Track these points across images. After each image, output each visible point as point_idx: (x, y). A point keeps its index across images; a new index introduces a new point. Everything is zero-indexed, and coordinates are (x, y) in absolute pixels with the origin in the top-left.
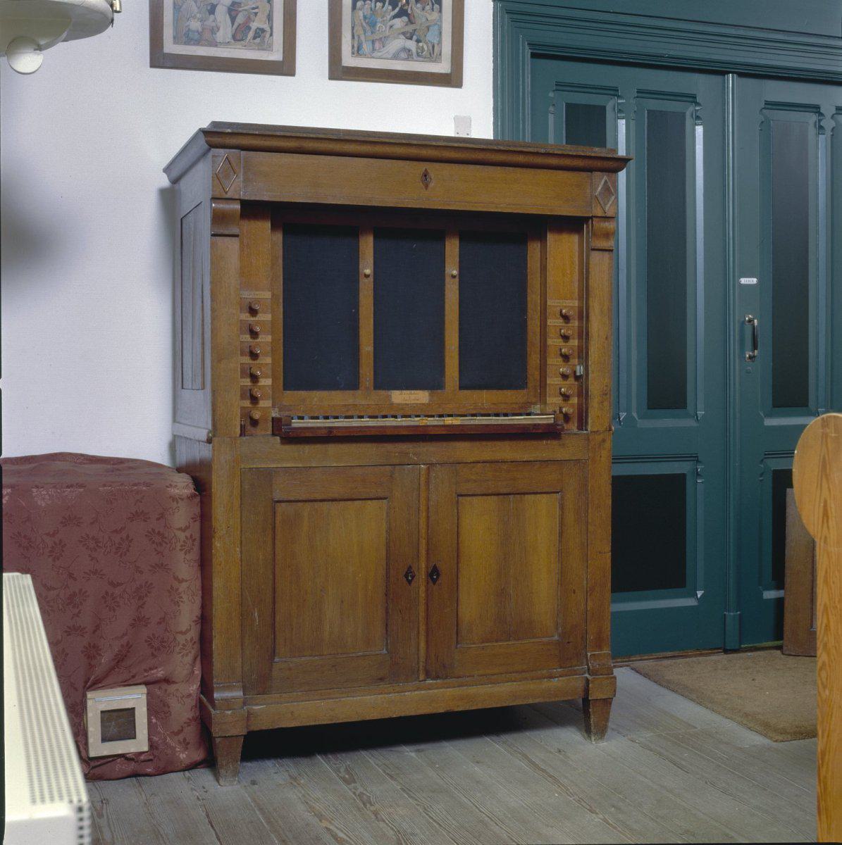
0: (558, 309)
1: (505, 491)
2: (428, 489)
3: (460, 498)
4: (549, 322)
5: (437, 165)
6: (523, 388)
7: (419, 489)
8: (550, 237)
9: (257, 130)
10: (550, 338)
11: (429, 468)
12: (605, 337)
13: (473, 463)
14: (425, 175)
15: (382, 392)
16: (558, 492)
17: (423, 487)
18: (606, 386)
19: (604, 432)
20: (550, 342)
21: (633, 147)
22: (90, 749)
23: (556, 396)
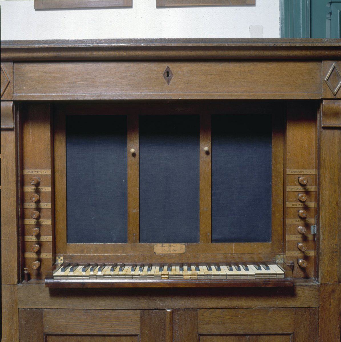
0: (297, 177)
1: (242, 332)
2: (173, 329)
3: (201, 337)
4: (289, 188)
5: (178, 65)
6: (269, 241)
7: (164, 329)
8: (26, 241)
9: (241, 42)
10: (289, 202)
11: (173, 311)
12: (335, 203)
13: (213, 308)
14: (168, 73)
15: (147, 245)
16: (290, 334)
17: (168, 327)
18: (336, 245)
19: (333, 284)
20: (289, 205)
21: (281, 36)
22: (139, 315)
23: (294, 250)
